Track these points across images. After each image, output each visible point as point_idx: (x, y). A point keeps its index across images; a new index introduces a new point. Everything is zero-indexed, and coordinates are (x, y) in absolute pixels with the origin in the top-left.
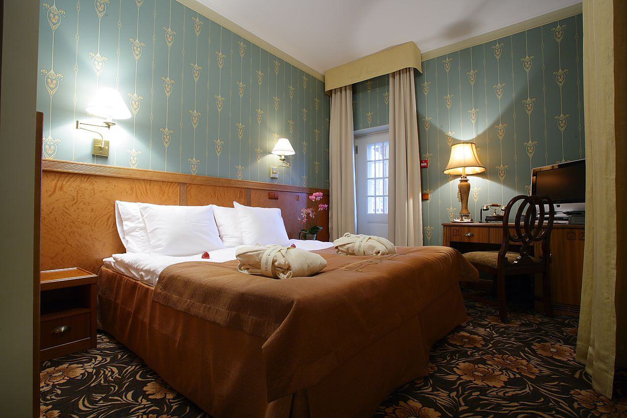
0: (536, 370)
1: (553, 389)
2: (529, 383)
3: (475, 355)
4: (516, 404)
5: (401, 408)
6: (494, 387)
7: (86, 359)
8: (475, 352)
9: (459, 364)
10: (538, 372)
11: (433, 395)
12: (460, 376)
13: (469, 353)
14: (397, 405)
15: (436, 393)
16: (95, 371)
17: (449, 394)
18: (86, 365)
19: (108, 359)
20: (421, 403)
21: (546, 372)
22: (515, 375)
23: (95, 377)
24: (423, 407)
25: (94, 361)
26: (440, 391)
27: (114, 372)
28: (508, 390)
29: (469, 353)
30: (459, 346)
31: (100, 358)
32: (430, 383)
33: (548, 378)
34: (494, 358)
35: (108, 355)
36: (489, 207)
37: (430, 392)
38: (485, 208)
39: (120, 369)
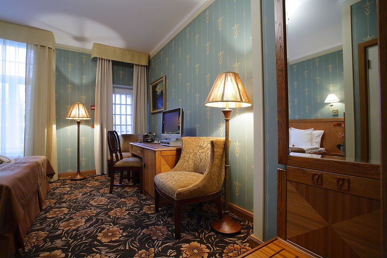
24: (50, 253)
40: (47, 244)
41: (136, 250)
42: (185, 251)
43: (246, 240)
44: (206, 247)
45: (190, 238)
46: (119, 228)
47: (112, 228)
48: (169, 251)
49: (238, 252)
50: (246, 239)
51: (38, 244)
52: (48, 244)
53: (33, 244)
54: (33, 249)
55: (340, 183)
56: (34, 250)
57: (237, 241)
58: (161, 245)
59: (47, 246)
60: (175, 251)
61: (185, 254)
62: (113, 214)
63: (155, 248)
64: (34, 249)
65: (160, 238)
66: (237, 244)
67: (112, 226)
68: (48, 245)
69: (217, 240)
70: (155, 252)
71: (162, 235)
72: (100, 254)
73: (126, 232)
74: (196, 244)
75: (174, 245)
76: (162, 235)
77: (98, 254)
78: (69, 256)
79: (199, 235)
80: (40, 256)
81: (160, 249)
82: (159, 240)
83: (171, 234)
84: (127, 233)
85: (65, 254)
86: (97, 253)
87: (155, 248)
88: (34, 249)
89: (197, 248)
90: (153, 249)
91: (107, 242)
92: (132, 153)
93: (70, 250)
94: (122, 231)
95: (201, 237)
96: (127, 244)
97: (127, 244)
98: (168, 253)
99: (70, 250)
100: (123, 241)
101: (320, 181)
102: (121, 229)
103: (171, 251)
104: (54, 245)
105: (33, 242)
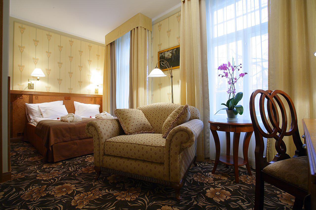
3: (217, 183)
5: (223, 198)
6: (169, 206)
7: (82, 175)
8: (216, 185)
9: (227, 179)
12: (228, 175)
13: (220, 184)
14: (225, 200)
15: (204, 205)
16: (78, 170)
17: (197, 203)
18: (82, 172)
19: (72, 174)
20: (213, 200)
23: (77, 168)
24: (213, 198)
25: (79, 174)
27: (71, 169)
29: (220, 184)
30: (224, 189)
31: (76, 175)
35: (72, 176)
39: (68, 170)
46: (279, 200)
47: (288, 205)
62: (27, 198)
67: (286, 207)
73: (274, 192)
78: (205, 188)
80: (220, 201)
84: (275, 191)
85: (206, 191)
92: (290, 158)
93: (202, 191)
94: (278, 196)
99: (202, 191)
102: (278, 198)
104: (207, 203)
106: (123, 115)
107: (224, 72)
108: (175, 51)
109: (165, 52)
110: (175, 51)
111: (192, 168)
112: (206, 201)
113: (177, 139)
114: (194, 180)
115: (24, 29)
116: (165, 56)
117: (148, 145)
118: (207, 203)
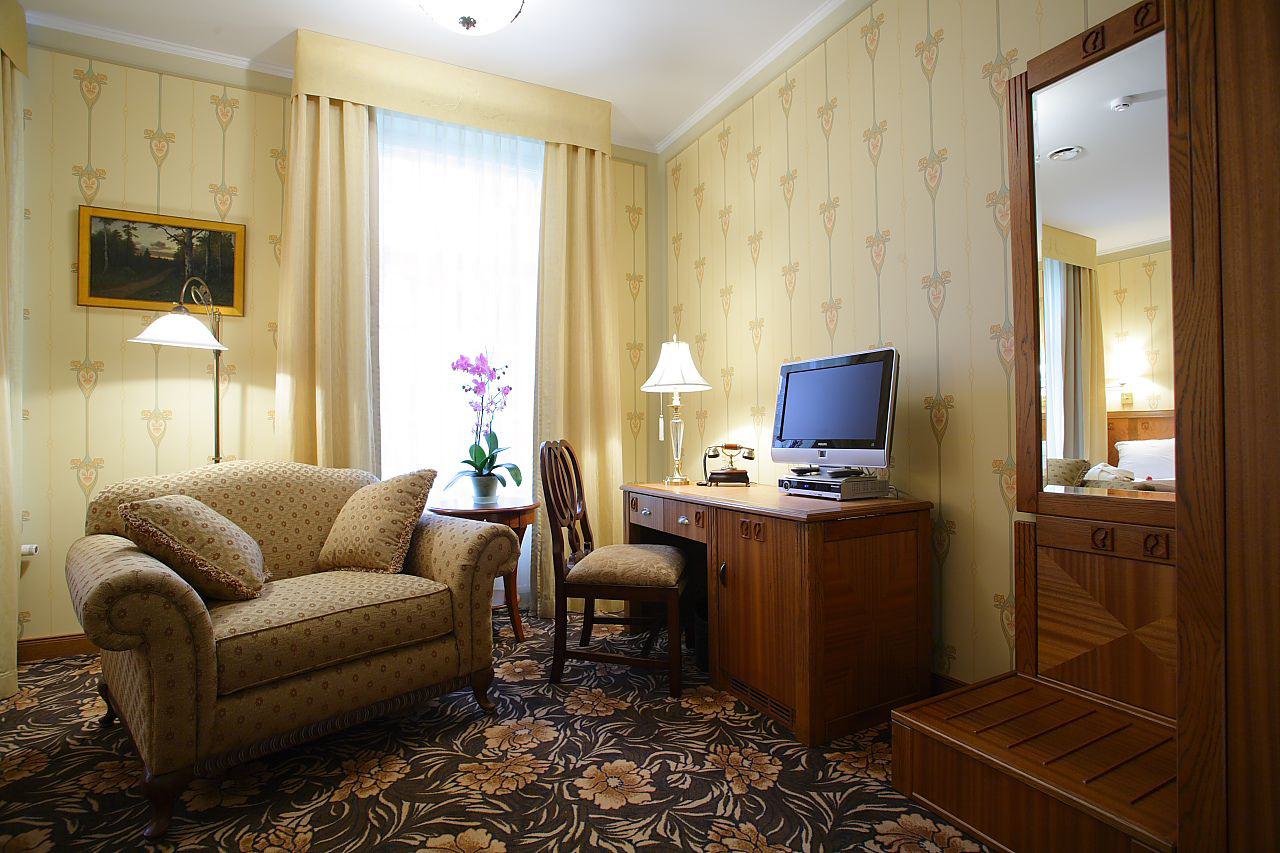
0: (464, 781)
1: (430, 760)
2: (460, 753)
4: (459, 721)
10: (458, 780)
11: (207, 831)
15: (205, 836)
21: (448, 787)
22: (484, 755)
26: (198, 844)
28: (476, 731)
32: (222, 847)
33: (443, 774)
34: (531, 770)
36: (720, 449)
37: (214, 833)
38: (711, 454)
40: (226, 835)
41: (381, 799)
42: (644, 782)
43: (850, 790)
44: (580, 792)
45: (618, 824)
48: (686, 786)
49: (874, 760)
50: (849, 795)
51: (256, 837)
52: (224, 833)
53: (272, 837)
54: (267, 820)
55: (1151, 542)
56: (265, 816)
57: (880, 788)
58: (714, 802)
59: (227, 828)
60: (671, 783)
61: (642, 777)
63: (730, 794)
64: (263, 821)
65: (726, 827)
66: (876, 780)
68: (224, 830)
69: (533, 811)
70: (728, 782)
71: (725, 841)
72: (484, 793)
74: (606, 802)
75: (676, 801)
76: (725, 841)
77: (489, 792)
79: (586, 834)
80: (246, 798)
81: (717, 793)
82: (726, 818)
83: (691, 844)
86: (494, 796)
87: (730, 794)
88: (263, 821)
89: (606, 790)
90: (737, 791)
91: (471, 829)
95: (582, 824)
96: (403, 818)
97: (403, 818)
98: (689, 780)
99: (575, 807)
100: (417, 829)
101: (1108, 542)
103: (683, 783)
104: (205, 828)
105: (271, 845)
106: (1071, 471)
107: (475, 381)
108: (201, 240)
109: (134, 222)
110: (201, 240)
111: (49, 762)
112: (203, 826)
113: (490, 557)
114: (99, 797)
115: (101, 80)
116: (134, 239)
117: (405, 600)
118: (205, 828)
